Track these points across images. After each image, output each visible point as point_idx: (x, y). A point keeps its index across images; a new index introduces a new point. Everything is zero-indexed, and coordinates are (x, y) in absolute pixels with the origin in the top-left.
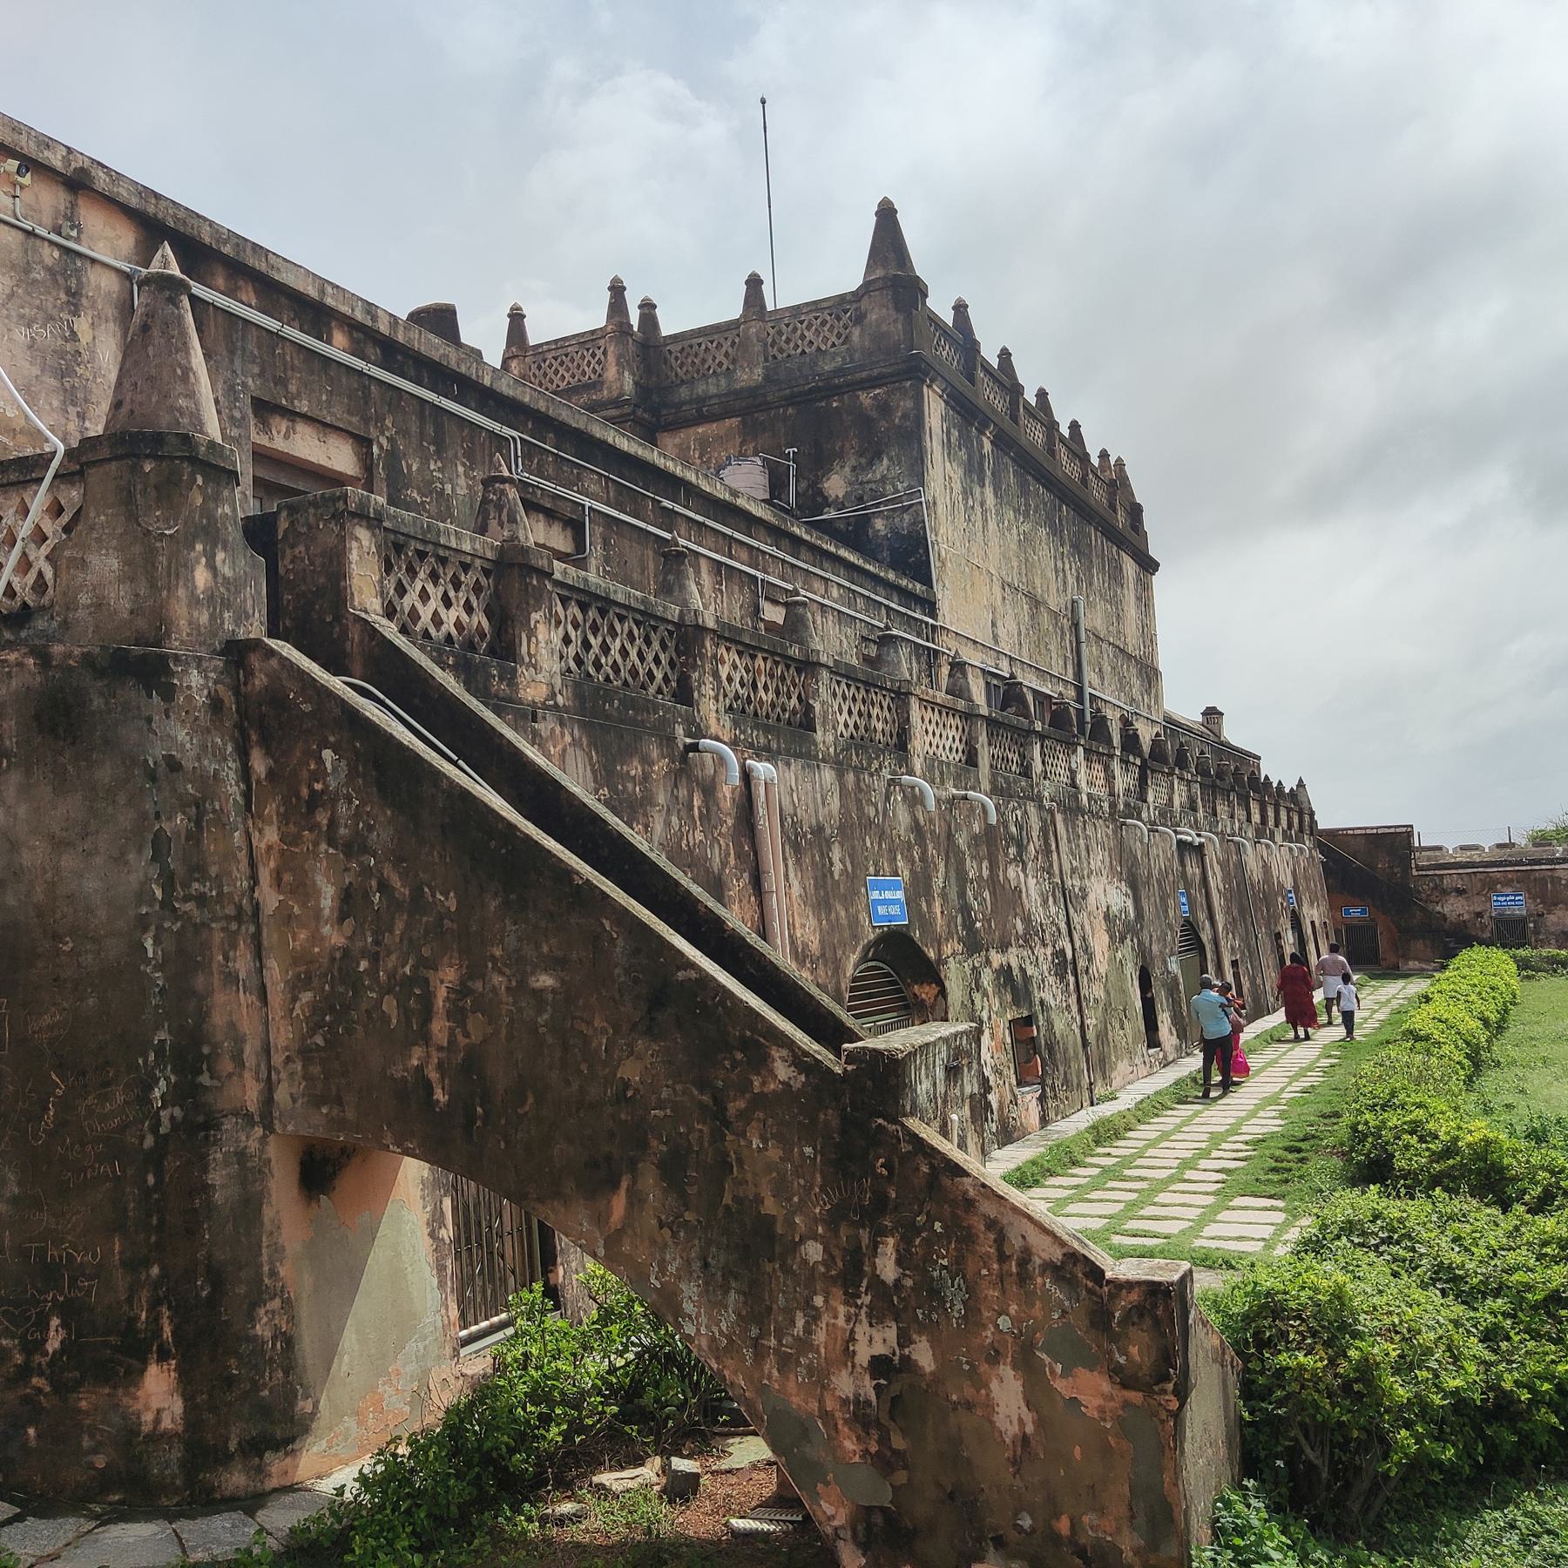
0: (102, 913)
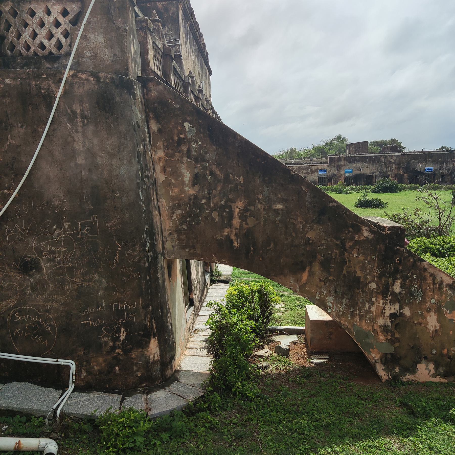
0: (127, 182)
